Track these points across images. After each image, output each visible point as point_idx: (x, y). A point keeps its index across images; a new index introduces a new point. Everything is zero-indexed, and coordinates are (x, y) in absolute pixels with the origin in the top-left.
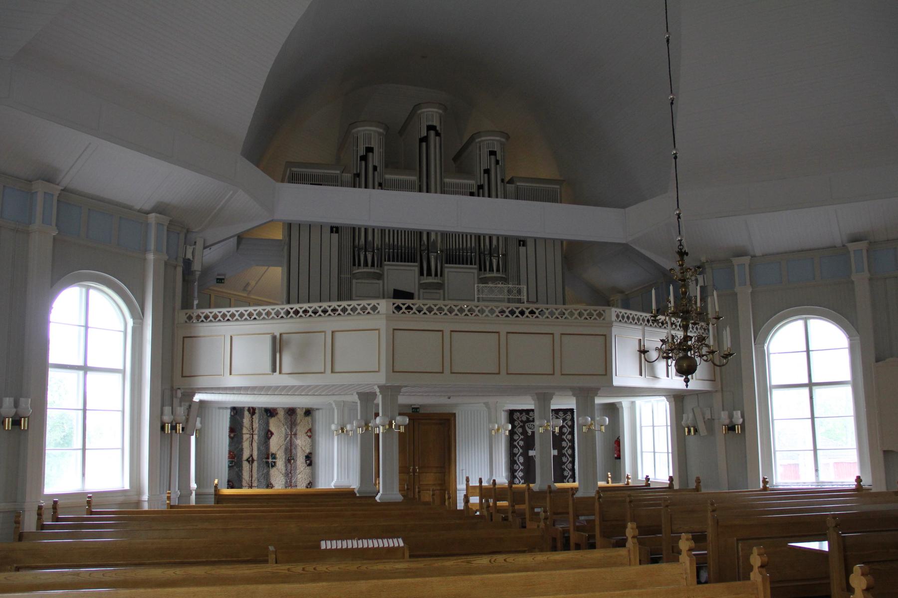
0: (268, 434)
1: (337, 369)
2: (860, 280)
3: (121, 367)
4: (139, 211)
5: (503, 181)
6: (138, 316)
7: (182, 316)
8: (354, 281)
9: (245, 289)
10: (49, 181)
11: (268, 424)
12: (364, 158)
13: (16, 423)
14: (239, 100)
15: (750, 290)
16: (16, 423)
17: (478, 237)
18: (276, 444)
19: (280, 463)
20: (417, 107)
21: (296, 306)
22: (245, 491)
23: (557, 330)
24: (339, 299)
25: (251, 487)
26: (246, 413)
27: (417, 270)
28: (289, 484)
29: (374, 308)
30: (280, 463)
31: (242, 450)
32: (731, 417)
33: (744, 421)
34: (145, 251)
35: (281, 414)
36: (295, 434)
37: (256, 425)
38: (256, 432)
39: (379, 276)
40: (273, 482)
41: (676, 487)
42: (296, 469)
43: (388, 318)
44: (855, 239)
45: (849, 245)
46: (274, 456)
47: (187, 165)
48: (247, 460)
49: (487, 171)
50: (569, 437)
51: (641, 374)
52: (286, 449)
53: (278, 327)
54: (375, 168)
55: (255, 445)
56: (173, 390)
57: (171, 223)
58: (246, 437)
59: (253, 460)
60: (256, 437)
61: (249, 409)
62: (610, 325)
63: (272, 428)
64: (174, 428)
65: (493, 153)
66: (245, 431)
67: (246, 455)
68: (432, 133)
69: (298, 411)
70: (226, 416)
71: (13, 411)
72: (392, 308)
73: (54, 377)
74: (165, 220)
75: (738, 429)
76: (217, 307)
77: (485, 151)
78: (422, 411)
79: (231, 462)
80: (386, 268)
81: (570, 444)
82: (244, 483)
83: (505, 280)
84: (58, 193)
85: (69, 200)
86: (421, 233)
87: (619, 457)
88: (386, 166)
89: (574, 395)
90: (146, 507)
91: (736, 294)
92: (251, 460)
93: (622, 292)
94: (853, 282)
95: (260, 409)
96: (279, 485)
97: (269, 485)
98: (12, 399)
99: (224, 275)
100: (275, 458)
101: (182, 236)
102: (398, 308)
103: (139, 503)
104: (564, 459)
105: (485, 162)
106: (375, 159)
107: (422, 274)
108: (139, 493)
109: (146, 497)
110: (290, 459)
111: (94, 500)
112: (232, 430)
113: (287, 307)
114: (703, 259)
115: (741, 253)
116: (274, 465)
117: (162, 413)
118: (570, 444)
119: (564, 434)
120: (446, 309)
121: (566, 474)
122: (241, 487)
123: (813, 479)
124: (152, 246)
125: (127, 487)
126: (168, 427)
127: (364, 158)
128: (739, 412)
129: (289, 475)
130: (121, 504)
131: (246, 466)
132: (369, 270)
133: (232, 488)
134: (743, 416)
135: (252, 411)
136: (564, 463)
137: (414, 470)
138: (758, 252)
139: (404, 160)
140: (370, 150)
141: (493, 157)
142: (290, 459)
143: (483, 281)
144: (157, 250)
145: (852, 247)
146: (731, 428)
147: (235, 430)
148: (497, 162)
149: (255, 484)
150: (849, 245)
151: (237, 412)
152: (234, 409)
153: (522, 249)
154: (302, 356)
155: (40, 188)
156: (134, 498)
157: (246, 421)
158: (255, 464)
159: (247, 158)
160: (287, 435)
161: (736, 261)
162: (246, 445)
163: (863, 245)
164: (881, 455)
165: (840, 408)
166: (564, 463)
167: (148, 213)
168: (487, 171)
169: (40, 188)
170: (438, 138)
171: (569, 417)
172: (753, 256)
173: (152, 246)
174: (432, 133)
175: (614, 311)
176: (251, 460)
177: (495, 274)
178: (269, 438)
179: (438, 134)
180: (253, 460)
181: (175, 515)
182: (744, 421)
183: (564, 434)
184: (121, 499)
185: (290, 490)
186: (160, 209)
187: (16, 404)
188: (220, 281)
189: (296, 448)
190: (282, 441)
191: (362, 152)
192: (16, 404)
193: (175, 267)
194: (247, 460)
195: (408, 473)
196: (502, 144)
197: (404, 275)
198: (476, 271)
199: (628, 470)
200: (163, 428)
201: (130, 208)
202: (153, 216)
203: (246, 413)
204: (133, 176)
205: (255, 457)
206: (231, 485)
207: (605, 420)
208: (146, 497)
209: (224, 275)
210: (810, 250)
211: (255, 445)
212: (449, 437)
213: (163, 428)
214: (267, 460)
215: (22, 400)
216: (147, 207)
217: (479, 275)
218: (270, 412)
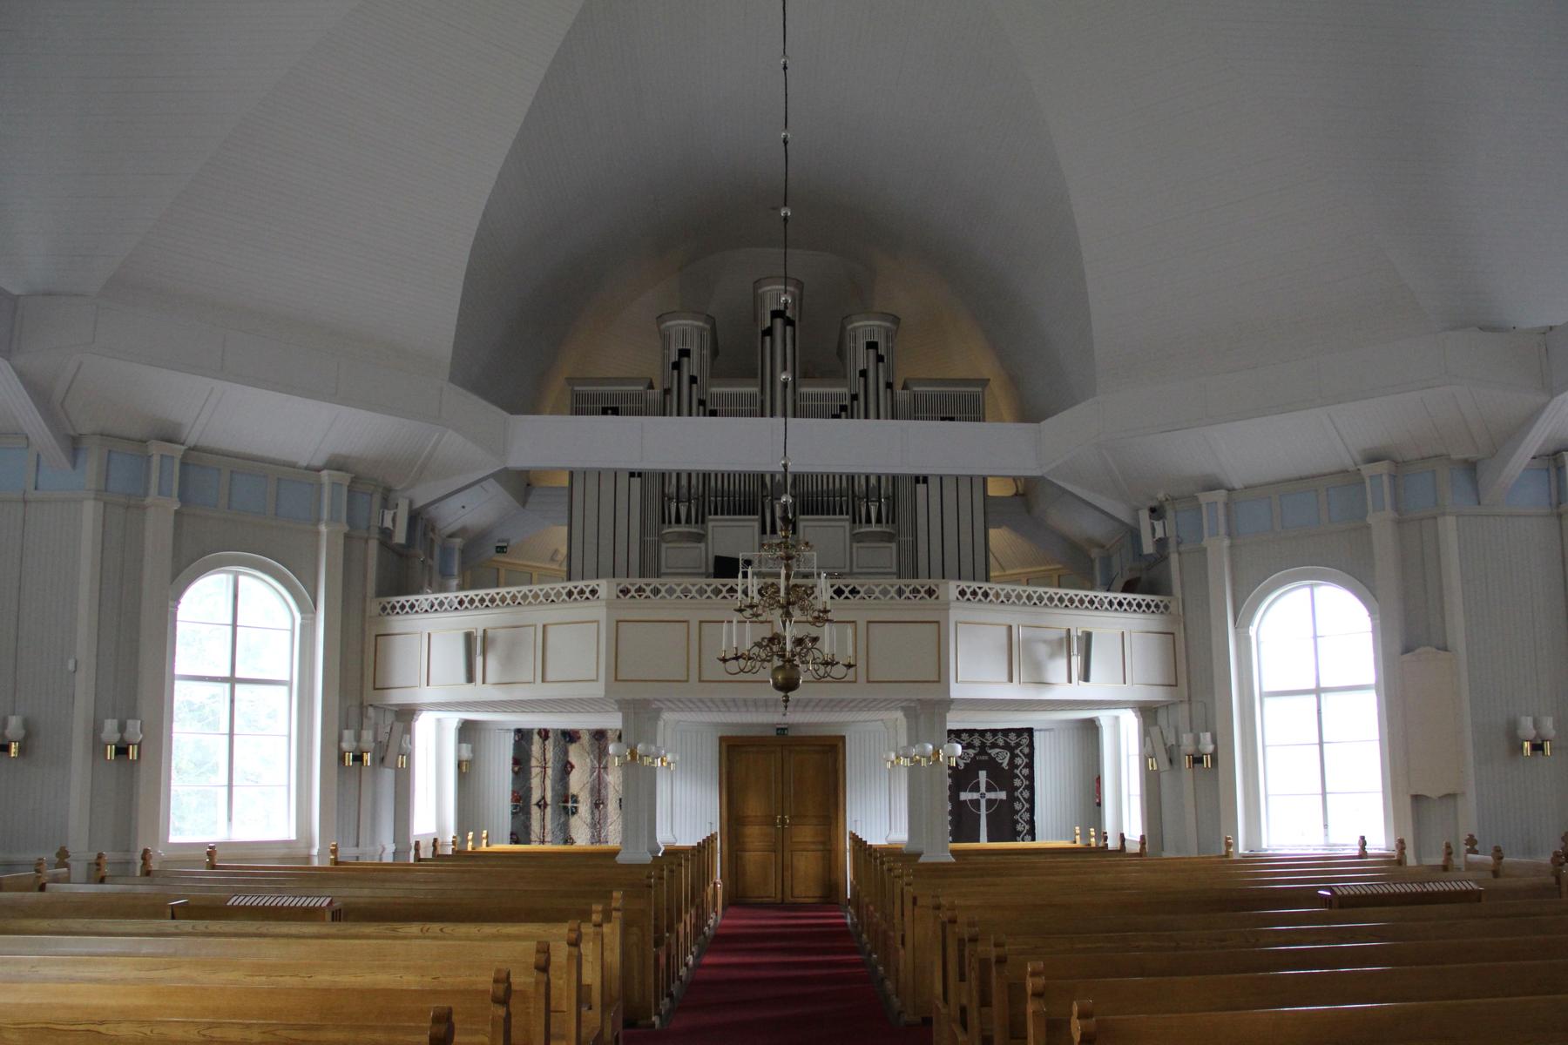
0: (566, 768)
1: (549, 677)
2: (1381, 522)
3: (287, 678)
4: (307, 468)
5: (889, 385)
6: (308, 609)
7: (374, 607)
8: (664, 546)
9: (552, 559)
10: (170, 441)
11: (566, 753)
12: (677, 366)
13: (122, 751)
14: (429, 304)
15: (1226, 542)
16: (122, 751)
17: (851, 478)
18: (578, 782)
19: (584, 808)
20: (757, 284)
21: (581, 584)
22: (534, 847)
23: (862, 618)
24: (642, 575)
25: (543, 842)
26: (536, 738)
27: (757, 525)
28: (597, 836)
29: (593, 592)
30: (584, 808)
31: (530, 789)
32: (1197, 741)
33: (1216, 750)
34: (318, 520)
35: (585, 739)
36: (605, 768)
37: (550, 755)
38: (550, 764)
39: (700, 538)
40: (573, 835)
41: (1411, 860)
42: (606, 818)
43: (609, 605)
44: (1373, 458)
45: (1362, 467)
46: (575, 799)
47: (346, 401)
48: (538, 804)
49: (864, 373)
50: (1026, 772)
51: (1011, 680)
52: (592, 790)
53: (477, 620)
54: (693, 380)
55: (548, 783)
56: (362, 708)
57: (355, 480)
58: (535, 771)
59: (545, 805)
60: (549, 771)
61: (539, 732)
62: (946, 607)
63: (573, 759)
64: (358, 758)
65: (872, 345)
66: (534, 762)
67: (536, 797)
68: (779, 322)
69: (610, 734)
70: (509, 741)
71: (117, 737)
72: (615, 591)
73: (183, 693)
74: (345, 478)
75: (1207, 761)
76: (508, 584)
77: (861, 343)
78: (791, 733)
79: (515, 807)
80: (710, 524)
81: (1026, 783)
82: (533, 837)
83: (890, 537)
84: (179, 455)
85: (197, 462)
86: (763, 476)
87: (1099, 804)
88: (712, 376)
89: (620, 709)
90: (316, 863)
91: (1205, 550)
92: (542, 805)
93: (1102, 547)
94: (1368, 527)
95: (555, 731)
96: (582, 839)
97: (568, 840)
98: (115, 722)
99: (507, 541)
100: (576, 801)
101: (377, 499)
102: (625, 592)
103: (309, 858)
104: (1017, 806)
105: (861, 358)
106: (691, 367)
107: (763, 531)
108: (310, 845)
109: (315, 851)
110: (598, 803)
111: (219, 852)
112: (516, 761)
113: (570, 585)
114: (1161, 496)
115: (1212, 485)
116: (575, 811)
117: (340, 739)
118: (1026, 783)
119: (1017, 767)
120: (679, 589)
121: (1019, 828)
122: (528, 842)
123: (1320, 840)
124: (325, 515)
125: (294, 837)
126: (349, 757)
127: (677, 366)
128: (1208, 735)
129: (597, 826)
130: (282, 859)
131: (535, 811)
132: (683, 528)
133: (517, 842)
134: (1214, 741)
135: (544, 734)
136: (1017, 812)
137: (783, 821)
138: (1237, 485)
139: (729, 365)
140: (684, 353)
141: (872, 352)
142: (598, 803)
143: (857, 538)
144: (333, 519)
145: (1367, 470)
146: (1197, 760)
147: (521, 762)
148: (880, 359)
149: (548, 838)
150: (1362, 467)
151: (523, 736)
152: (518, 731)
153: (921, 488)
154: (509, 660)
155: (156, 449)
156: (303, 852)
157: (536, 748)
158: (549, 810)
159: (463, 386)
160: (593, 768)
161: (1204, 498)
162: (535, 782)
163: (1382, 467)
164: (1408, 800)
165: (1359, 727)
166: (1017, 812)
167: (319, 470)
168: (864, 373)
169: (156, 449)
170: (789, 329)
171: (1025, 741)
172: (1231, 490)
173: (325, 515)
174: (779, 322)
175: (952, 588)
176: (542, 805)
177: (874, 528)
178: (568, 773)
179: (789, 322)
180: (545, 805)
181: (339, 871)
182: (1216, 750)
183: (1017, 767)
184: (283, 852)
185: (597, 847)
186: (337, 464)
187: (122, 728)
188: (501, 550)
189: (606, 787)
190: (586, 778)
191: (674, 357)
192: (122, 728)
193: (367, 541)
194: (538, 804)
195: (775, 824)
196: (887, 330)
197: (734, 535)
198: (847, 525)
199: (1109, 826)
200: (342, 758)
201: (293, 465)
202: (324, 473)
203: (536, 738)
204: (294, 426)
205: (549, 800)
206: (515, 839)
207: (954, 749)
208: (315, 851)
209: (507, 541)
210: (1313, 477)
211: (548, 783)
212: (836, 771)
213: (342, 758)
214: (566, 804)
215: (130, 722)
216: (318, 461)
217: (852, 529)
218: (570, 736)
